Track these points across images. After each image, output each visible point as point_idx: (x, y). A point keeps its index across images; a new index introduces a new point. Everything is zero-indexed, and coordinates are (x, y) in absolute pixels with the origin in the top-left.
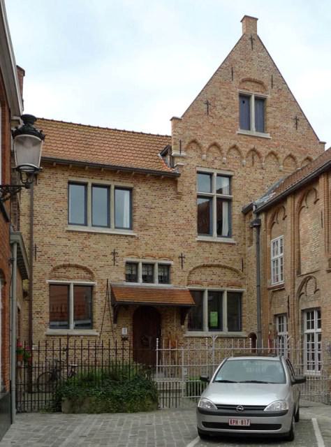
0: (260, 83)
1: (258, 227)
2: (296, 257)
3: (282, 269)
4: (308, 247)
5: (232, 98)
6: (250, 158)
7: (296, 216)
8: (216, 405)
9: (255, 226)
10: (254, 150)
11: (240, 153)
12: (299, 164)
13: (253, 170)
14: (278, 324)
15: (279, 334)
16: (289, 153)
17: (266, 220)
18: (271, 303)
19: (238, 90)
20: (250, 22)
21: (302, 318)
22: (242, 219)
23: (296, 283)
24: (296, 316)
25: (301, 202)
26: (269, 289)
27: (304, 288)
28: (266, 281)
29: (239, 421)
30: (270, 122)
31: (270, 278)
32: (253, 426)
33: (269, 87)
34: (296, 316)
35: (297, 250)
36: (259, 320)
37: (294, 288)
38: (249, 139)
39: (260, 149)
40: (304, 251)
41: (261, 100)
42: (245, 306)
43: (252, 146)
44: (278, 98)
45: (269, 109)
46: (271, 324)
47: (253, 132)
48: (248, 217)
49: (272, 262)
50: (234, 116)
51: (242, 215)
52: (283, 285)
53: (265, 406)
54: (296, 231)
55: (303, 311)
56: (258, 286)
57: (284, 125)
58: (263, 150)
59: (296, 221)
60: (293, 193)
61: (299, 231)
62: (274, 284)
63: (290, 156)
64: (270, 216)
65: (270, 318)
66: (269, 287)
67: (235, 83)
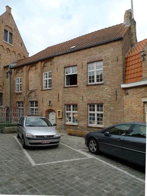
0: (11, 29)
1: (11, 73)
2: (27, 84)
3: (18, 88)
4: (32, 82)
5: (2, 30)
6: (7, 51)
7: (28, 72)
8: (35, 136)
9: (10, 73)
10: (8, 48)
11: (4, 48)
12: (22, 57)
13: (8, 55)
14: (18, 105)
15: (18, 108)
16: (19, 53)
17: (14, 71)
18: (15, 98)
19: (4, 28)
20: (8, 8)
21: (29, 103)
22: (3, 69)
23: (27, 92)
24: (27, 102)
25: (45, 64)
26: (15, 93)
27: (30, 94)
28: (14, 90)
29: (46, 141)
30: (14, 42)
31: (15, 89)
32: (51, 143)
33: (14, 31)
34: (27, 102)
35: (27, 82)
36: (10, 102)
37: (26, 94)
38: (7, 44)
39: (10, 49)
40: (30, 83)
41: (11, 34)
42: (4, 98)
43: (8, 47)
44: (16, 35)
45: (13, 38)
46: (15, 104)
47: (8, 42)
48: (6, 69)
49: (44, 81)
50: (2, 35)
51: (4, 68)
52: (21, 93)
53: (54, 135)
54: (27, 76)
55: (29, 101)
56: (10, 92)
57: (18, 44)
58: (11, 49)
59: (28, 73)
60: (42, 61)
61: (28, 77)
62: (17, 92)
63: (19, 54)
64: (15, 71)
65: (15, 103)
66: (15, 92)
67: (3, 25)
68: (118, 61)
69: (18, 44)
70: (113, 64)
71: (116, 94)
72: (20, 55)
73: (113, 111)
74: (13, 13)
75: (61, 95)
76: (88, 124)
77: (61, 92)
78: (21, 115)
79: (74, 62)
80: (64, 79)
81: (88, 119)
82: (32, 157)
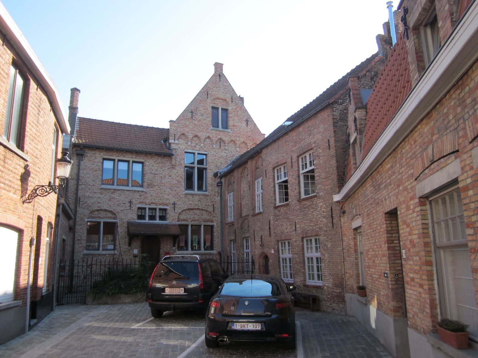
10: (220, 139)
11: (212, 141)
26: (227, 224)
33: (230, 102)
41: (225, 110)
43: (220, 137)
44: (236, 109)
57: (239, 124)
68: (329, 149)
69: (239, 124)
70: (325, 156)
71: (332, 214)
72: (246, 144)
73: (331, 250)
74: (226, 72)
75: (272, 222)
76: (305, 280)
77: (272, 219)
78: (288, 267)
79: (283, 156)
80: (299, 183)
81: (305, 269)
82: (177, 330)
